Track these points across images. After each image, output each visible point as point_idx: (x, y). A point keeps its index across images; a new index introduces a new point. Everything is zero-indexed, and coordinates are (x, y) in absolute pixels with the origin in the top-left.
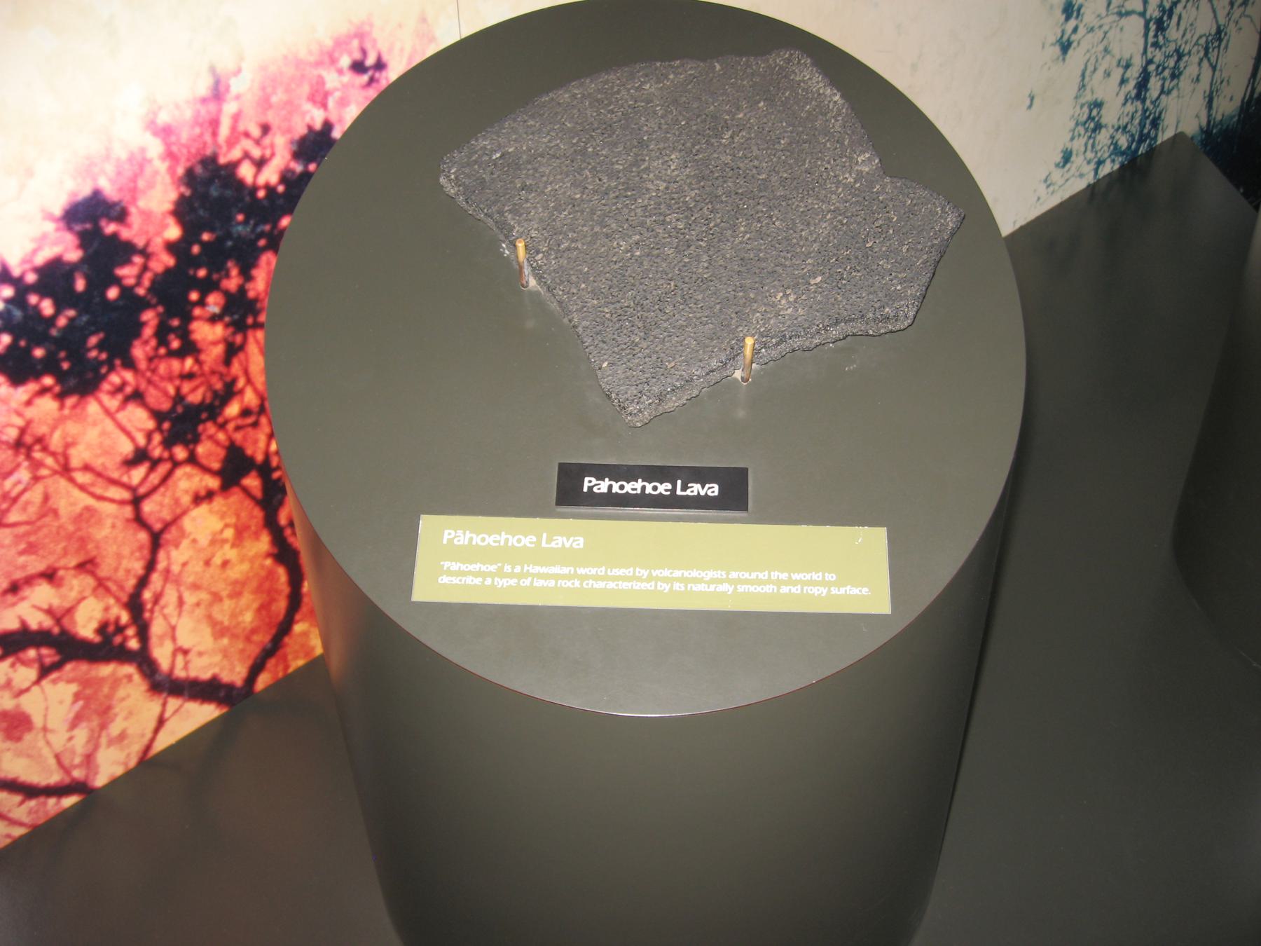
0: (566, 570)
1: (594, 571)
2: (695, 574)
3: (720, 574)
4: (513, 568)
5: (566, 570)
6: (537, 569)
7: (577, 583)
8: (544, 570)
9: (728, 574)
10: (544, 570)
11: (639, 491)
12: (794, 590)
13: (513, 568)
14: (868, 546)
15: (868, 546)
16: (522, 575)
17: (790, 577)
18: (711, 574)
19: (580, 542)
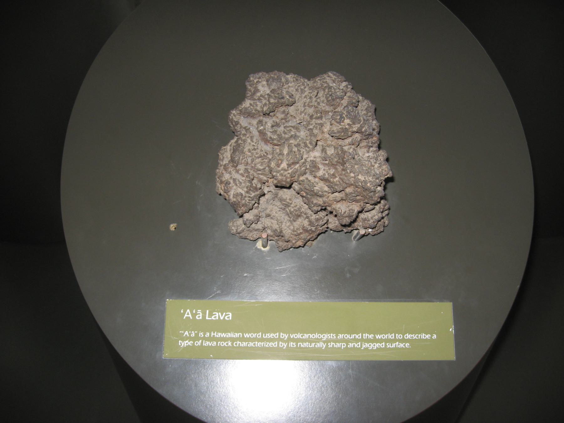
0: (237, 335)
1: (254, 335)
2: (316, 336)
3: (332, 336)
4: (204, 334)
5: (237, 335)
6: (220, 335)
7: (201, 334)
8: (224, 335)
9: (337, 336)
10: (224, 335)
11: (217, 318)
12: (356, 345)
13: (204, 334)
14: (442, 312)
15: (442, 312)
16: (197, 338)
17: (375, 337)
18: (325, 337)
19: (229, 316)
